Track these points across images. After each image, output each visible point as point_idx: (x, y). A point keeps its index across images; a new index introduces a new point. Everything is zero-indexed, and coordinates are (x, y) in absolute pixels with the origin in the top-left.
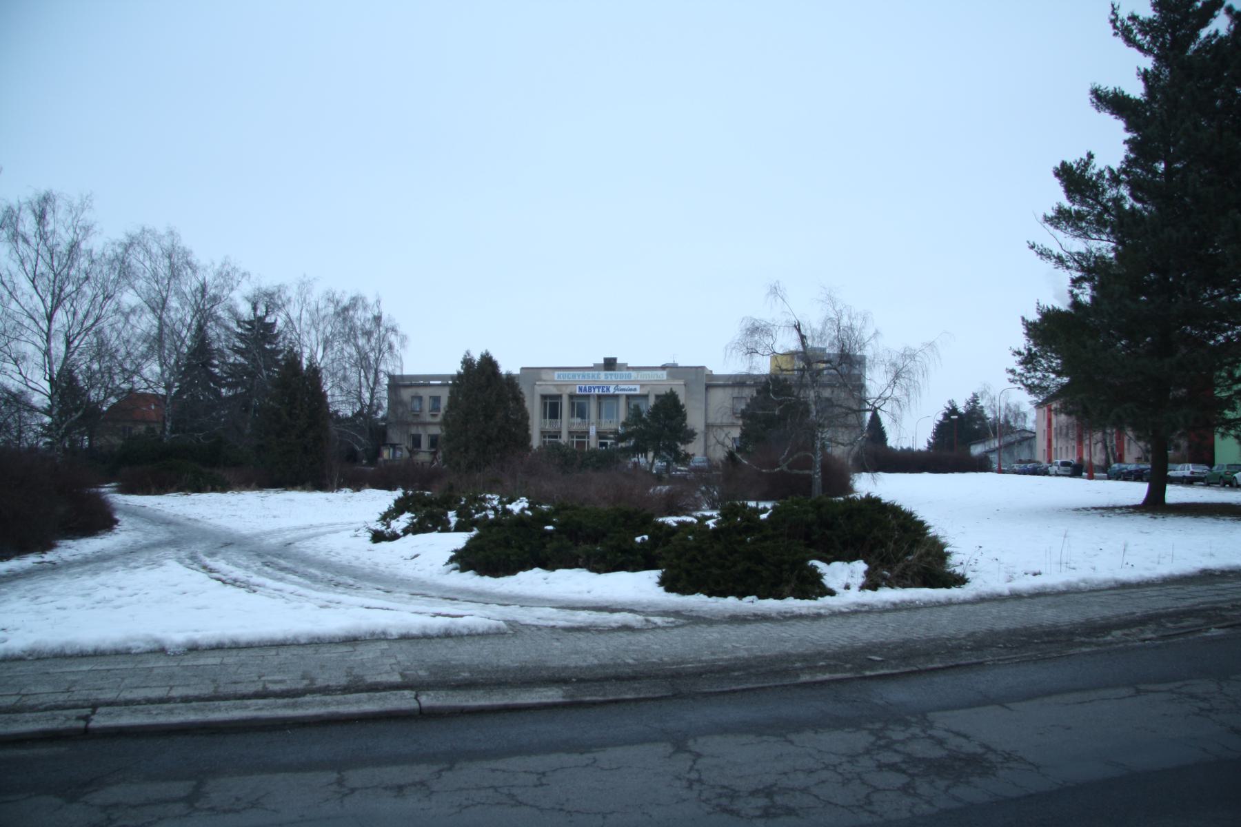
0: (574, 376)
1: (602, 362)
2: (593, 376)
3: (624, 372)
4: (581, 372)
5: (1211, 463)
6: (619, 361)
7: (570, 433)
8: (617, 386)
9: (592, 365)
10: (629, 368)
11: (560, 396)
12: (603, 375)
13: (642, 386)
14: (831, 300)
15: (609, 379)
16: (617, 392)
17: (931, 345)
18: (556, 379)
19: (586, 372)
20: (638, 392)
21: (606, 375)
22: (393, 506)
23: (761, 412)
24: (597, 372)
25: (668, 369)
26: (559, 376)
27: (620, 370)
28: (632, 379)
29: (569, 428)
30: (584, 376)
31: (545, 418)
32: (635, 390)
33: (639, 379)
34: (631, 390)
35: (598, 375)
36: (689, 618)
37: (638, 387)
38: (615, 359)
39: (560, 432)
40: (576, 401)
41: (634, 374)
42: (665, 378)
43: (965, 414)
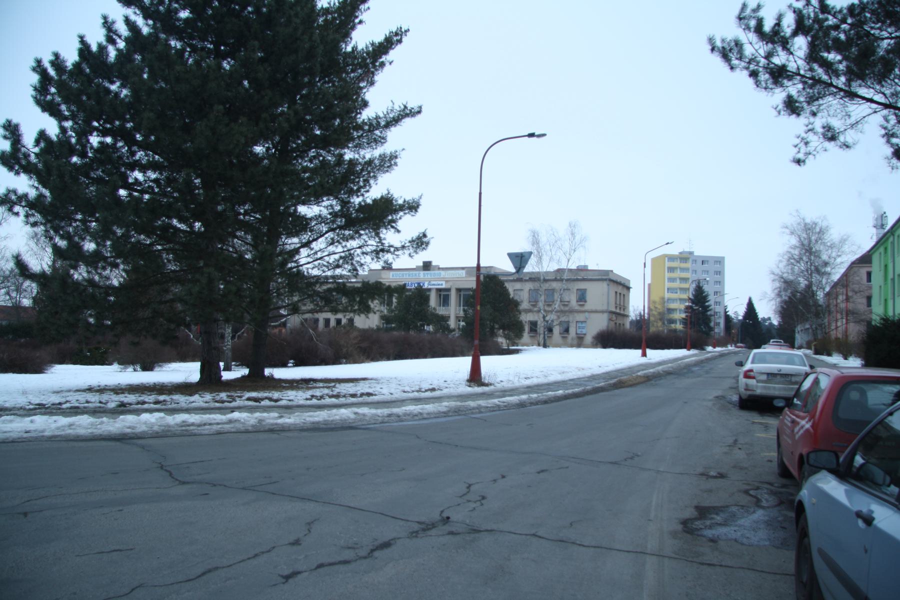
0: (403, 275)
1: (422, 264)
2: (416, 275)
3: (436, 272)
4: (407, 272)
5: (223, 370)
6: (434, 264)
7: (457, 317)
8: (430, 282)
9: (415, 267)
10: (439, 269)
11: (449, 290)
12: (422, 275)
13: (447, 281)
14: (420, 198)
15: (426, 277)
16: (430, 287)
17: (708, 261)
18: (391, 277)
19: (411, 272)
20: (443, 287)
21: (424, 274)
22: (865, 338)
23: (801, 308)
24: (418, 272)
25: (466, 269)
26: (393, 276)
27: (434, 270)
28: (442, 276)
29: (456, 314)
30: (409, 275)
31: (460, 306)
32: (442, 285)
33: (446, 276)
34: (439, 285)
35: (419, 274)
36: (246, 489)
37: (444, 283)
38: (430, 262)
39: (449, 317)
40: (442, 293)
41: (443, 273)
42: (464, 276)
43: (509, 299)
